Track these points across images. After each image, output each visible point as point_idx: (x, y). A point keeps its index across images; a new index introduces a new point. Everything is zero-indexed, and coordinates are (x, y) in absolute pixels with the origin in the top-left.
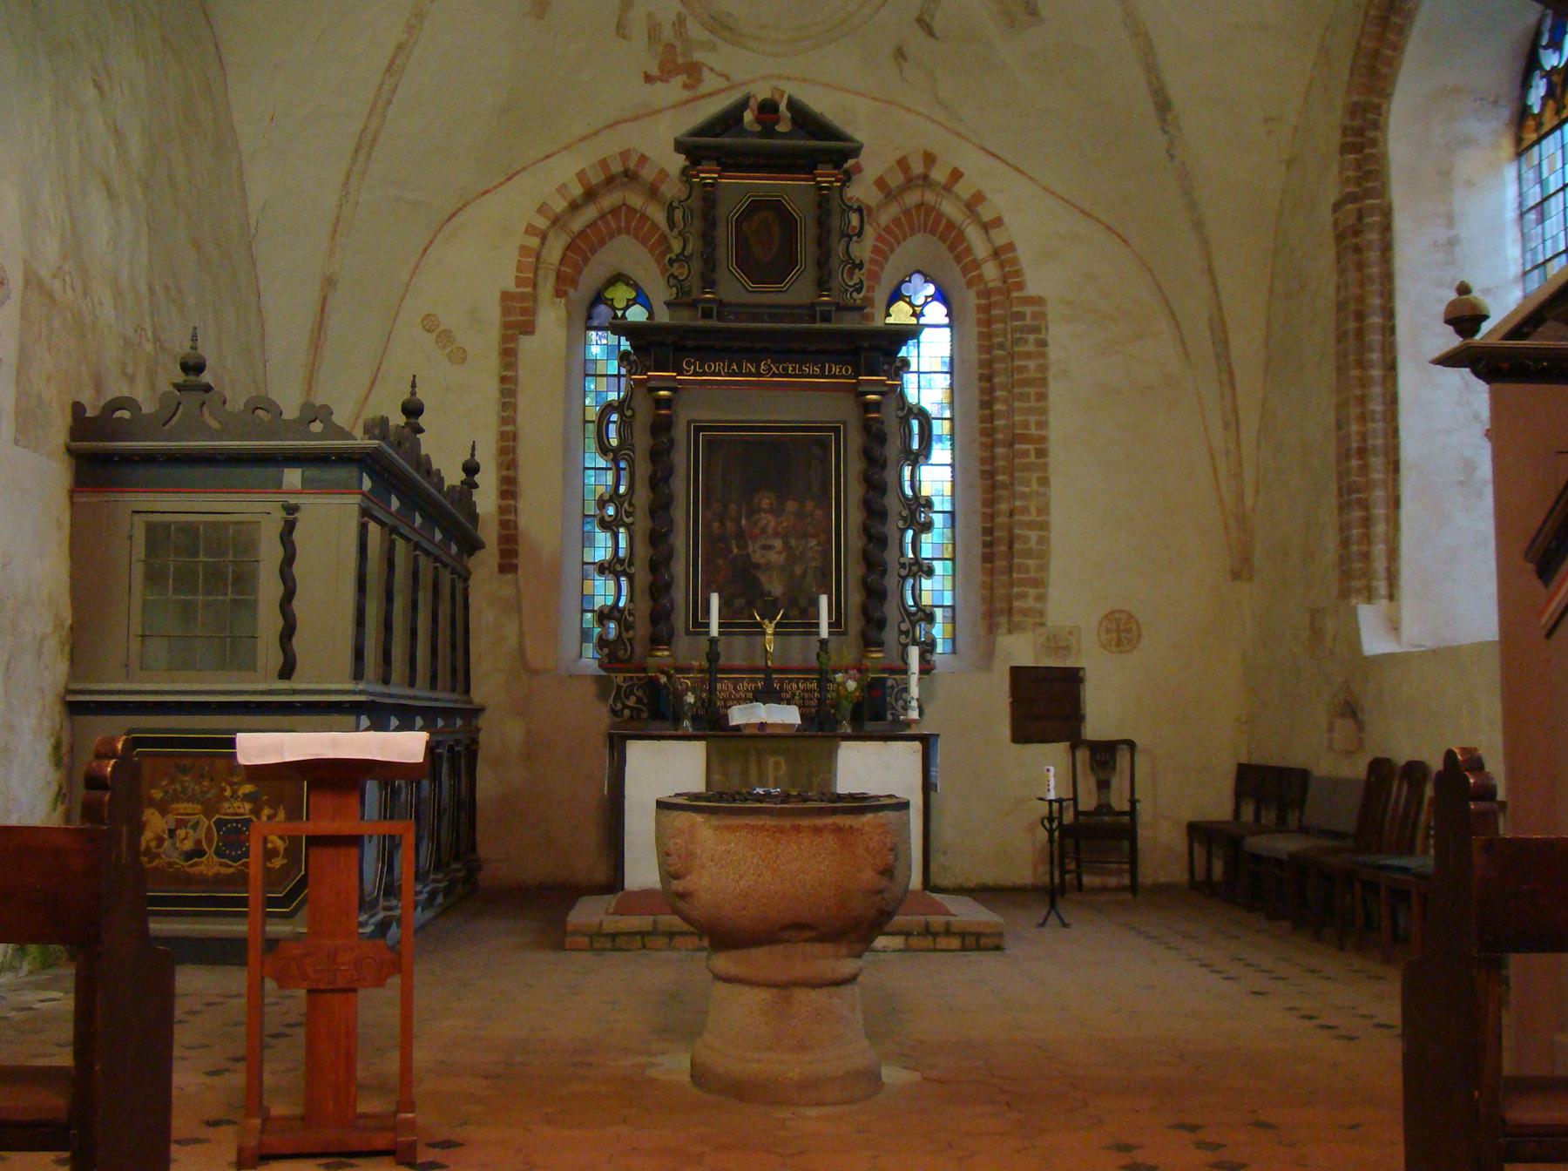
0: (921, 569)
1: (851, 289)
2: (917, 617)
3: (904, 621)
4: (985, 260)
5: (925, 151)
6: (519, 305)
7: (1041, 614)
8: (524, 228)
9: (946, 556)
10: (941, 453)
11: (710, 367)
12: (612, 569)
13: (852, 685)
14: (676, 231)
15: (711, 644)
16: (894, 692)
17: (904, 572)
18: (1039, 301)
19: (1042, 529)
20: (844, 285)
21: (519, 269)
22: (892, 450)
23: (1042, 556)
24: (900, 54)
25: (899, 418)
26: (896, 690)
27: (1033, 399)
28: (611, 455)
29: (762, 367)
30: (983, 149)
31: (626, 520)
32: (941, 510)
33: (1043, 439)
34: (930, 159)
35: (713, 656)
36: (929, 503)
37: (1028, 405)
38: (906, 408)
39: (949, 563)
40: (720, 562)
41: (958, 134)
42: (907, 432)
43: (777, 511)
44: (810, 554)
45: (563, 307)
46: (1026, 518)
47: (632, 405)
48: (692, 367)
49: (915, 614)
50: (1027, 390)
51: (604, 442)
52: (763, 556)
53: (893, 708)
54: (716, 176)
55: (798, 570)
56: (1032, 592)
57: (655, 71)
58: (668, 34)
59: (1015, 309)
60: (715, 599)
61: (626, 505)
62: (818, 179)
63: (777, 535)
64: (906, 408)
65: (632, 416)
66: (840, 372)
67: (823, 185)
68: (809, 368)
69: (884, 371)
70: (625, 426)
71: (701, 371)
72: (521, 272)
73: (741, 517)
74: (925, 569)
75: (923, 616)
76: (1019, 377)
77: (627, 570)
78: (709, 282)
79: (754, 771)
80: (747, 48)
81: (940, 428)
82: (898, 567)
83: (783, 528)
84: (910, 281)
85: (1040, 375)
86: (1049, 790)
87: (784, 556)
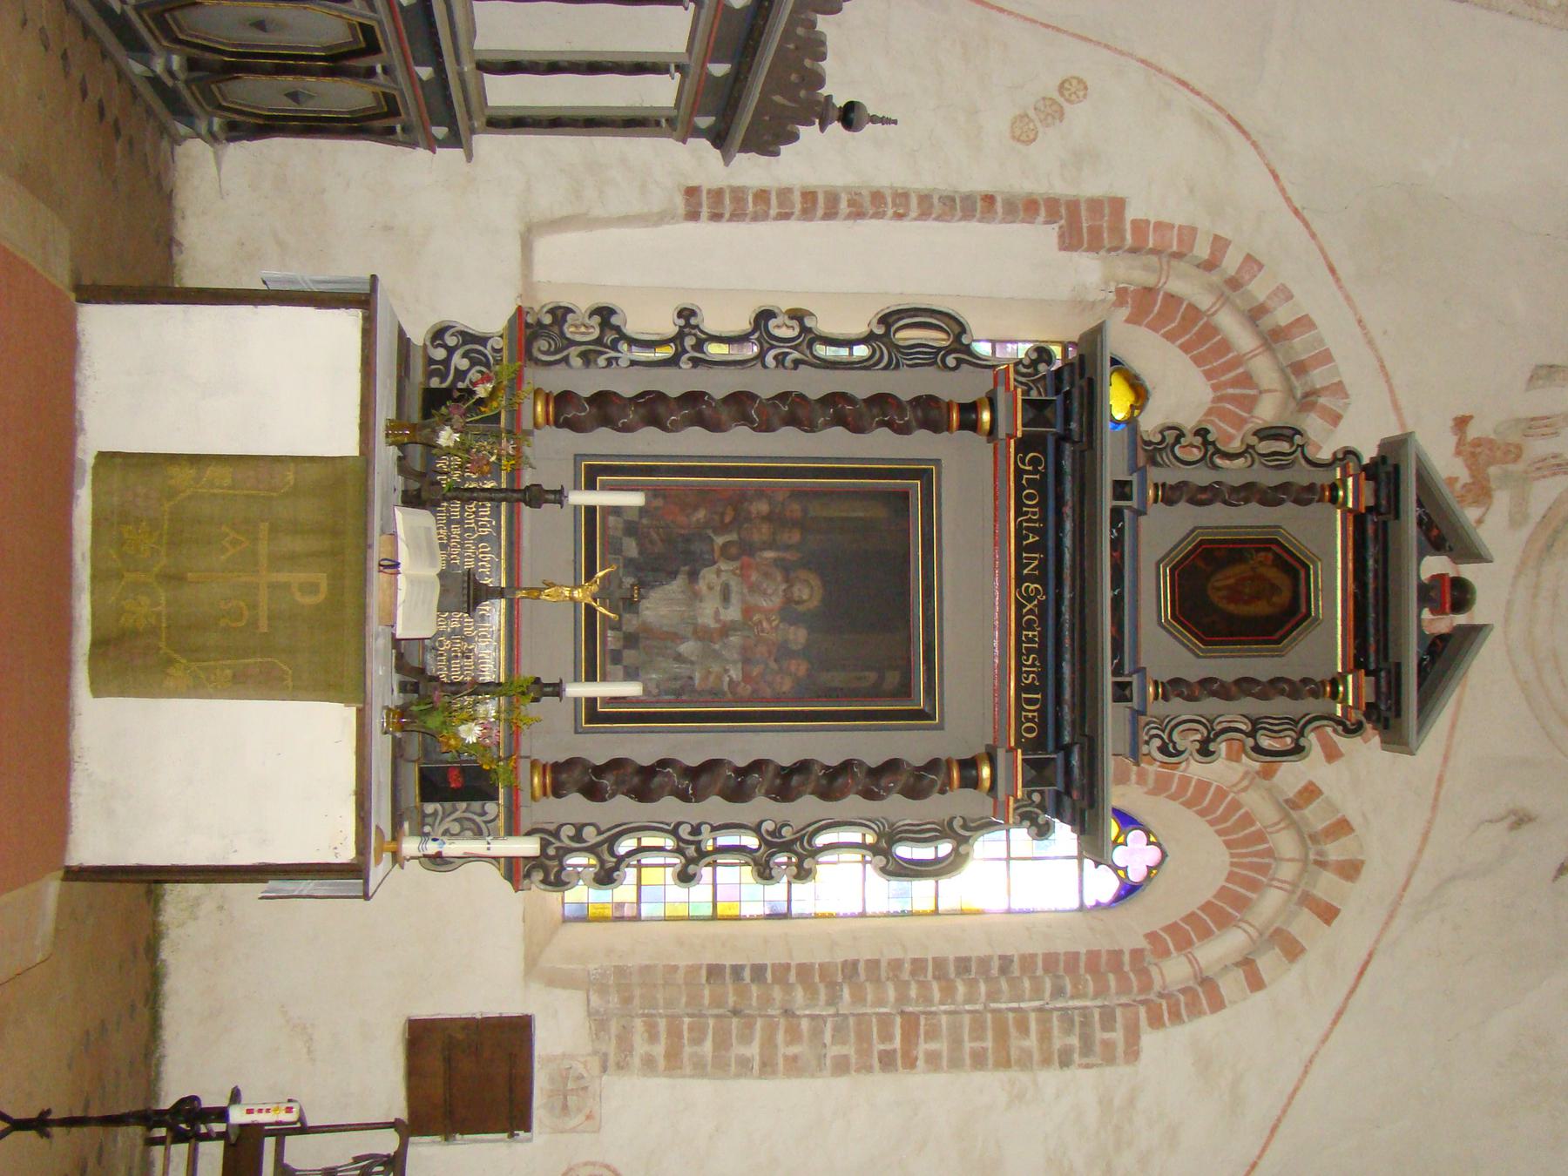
0: (690, 861)
1: (1165, 737)
2: (607, 857)
3: (600, 833)
4: (1193, 961)
5: (1362, 862)
6: (1105, 225)
7: (621, 1067)
8: (1222, 235)
9: (719, 906)
10: (885, 894)
11: (1029, 497)
12: (686, 330)
13: (471, 733)
14: (1253, 440)
15: (554, 492)
16: (475, 817)
17: (684, 831)
18: (1133, 1053)
19: (764, 1065)
20: (1173, 723)
21: (1159, 225)
22: (897, 808)
23: (720, 1066)
24: (1521, 820)
25: (952, 820)
26: (478, 819)
27: (976, 1045)
28: (880, 331)
29: (1032, 586)
30: (1370, 955)
31: (773, 353)
32: (793, 898)
33: (911, 1063)
34: (1351, 870)
35: (536, 496)
36: (803, 874)
37: (966, 1038)
38: (967, 834)
39: (708, 911)
40: (701, 514)
41: (1391, 916)
42: (927, 835)
43: (789, 611)
44: (716, 668)
45: (1102, 296)
46: (780, 1037)
47: (964, 367)
48: (1030, 468)
49: (612, 853)
50: (990, 1034)
51: (903, 318)
52: (710, 588)
53: (445, 816)
54: (1350, 505)
55: (688, 648)
56: (659, 1050)
57: (1473, 432)
58: (1539, 447)
59: (1119, 1012)
60: (635, 499)
61: (796, 355)
62: (1350, 678)
63: (748, 611)
64: (967, 834)
65: (945, 366)
66: (1026, 717)
67: (267, 1128)
68: (1033, 665)
69: (1029, 795)
70: (934, 357)
71: (1024, 482)
72: (1155, 228)
73: (778, 549)
74: (692, 869)
75: (609, 865)
76: (1011, 1022)
77: (687, 356)
78: (1171, 495)
79: (298, 545)
80: (1516, 577)
81: (920, 893)
82: (694, 823)
83: (760, 622)
84: (1149, 843)
85: (1014, 1054)
86: (250, 1111)
87: (713, 625)
